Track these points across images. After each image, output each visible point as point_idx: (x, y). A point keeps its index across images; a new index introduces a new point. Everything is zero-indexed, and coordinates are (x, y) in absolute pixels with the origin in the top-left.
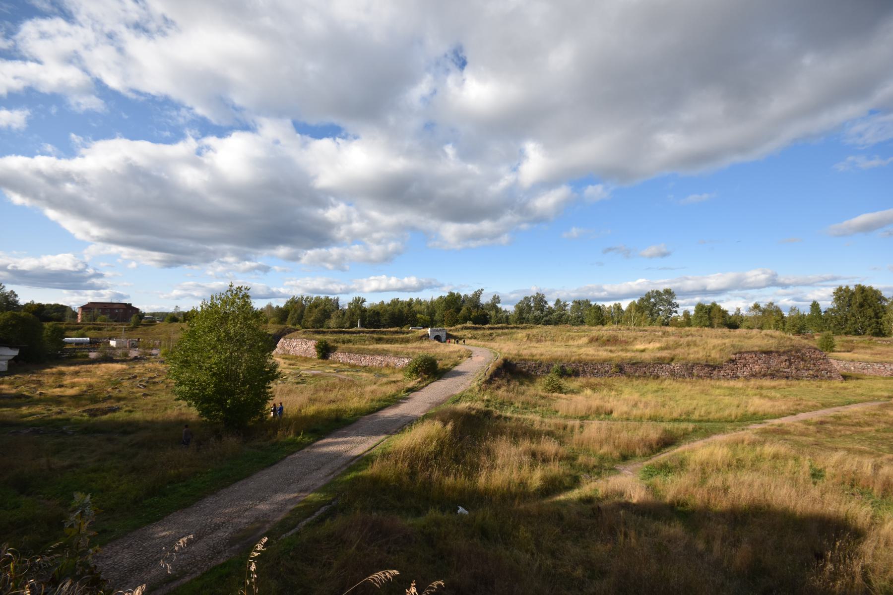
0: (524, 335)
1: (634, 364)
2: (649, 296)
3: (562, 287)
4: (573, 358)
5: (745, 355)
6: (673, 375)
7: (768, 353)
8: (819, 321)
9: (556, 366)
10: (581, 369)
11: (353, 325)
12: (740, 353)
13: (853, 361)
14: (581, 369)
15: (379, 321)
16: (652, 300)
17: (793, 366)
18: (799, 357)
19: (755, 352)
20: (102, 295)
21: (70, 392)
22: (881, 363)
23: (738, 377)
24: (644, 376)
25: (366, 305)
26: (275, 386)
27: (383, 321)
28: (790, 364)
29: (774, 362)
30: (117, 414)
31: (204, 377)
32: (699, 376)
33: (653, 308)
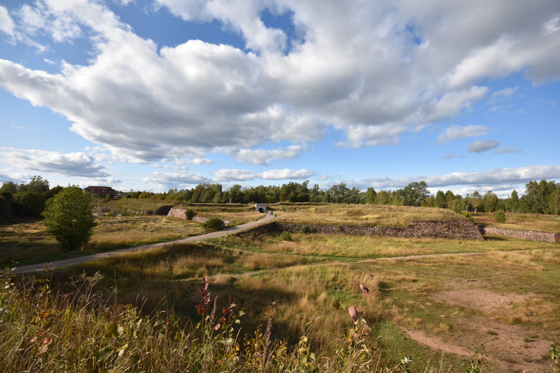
0: (314, 209)
1: (351, 227)
2: (410, 186)
3: (357, 178)
4: (315, 223)
5: (420, 223)
6: (373, 234)
7: (435, 222)
8: (516, 203)
9: (303, 227)
10: (318, 229)
11: (227, 201)
12: (417, 222)
13: (506, 229)
14: (318, 229)
15: (243, 199)
16: (413, 188)
17: (450, 231)
18: (455, 225)
19: (427, 222)
20: (106, 181)
21: (337, 263)
22: (522, 230)
23: (414, 236)
24: (355, 234)
25: (242, 190)
26: (95, 229)
27: (245, 199)
28: (449, 229)
29: (438, 228)
30: (43, 240)
31: (55, 223)
32: (389, 234)
33: (412, 195)
